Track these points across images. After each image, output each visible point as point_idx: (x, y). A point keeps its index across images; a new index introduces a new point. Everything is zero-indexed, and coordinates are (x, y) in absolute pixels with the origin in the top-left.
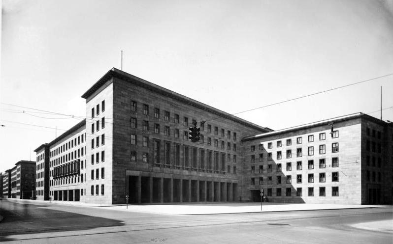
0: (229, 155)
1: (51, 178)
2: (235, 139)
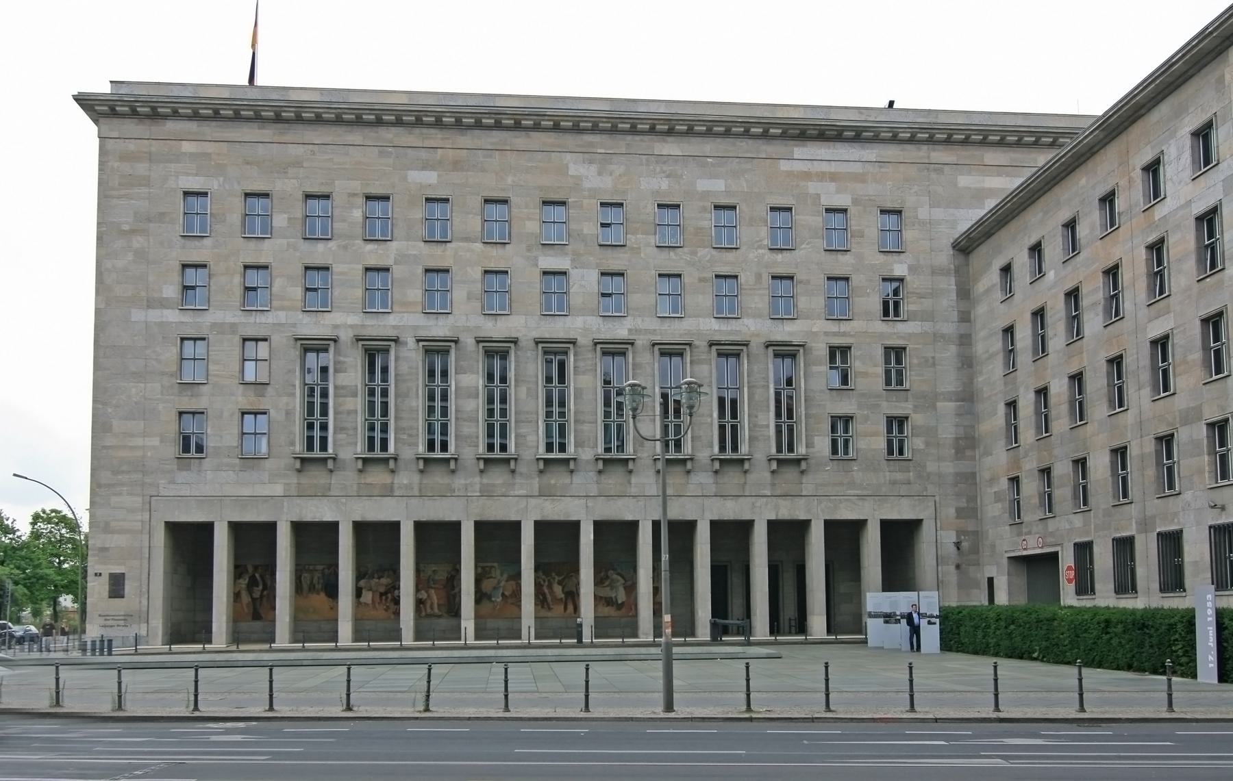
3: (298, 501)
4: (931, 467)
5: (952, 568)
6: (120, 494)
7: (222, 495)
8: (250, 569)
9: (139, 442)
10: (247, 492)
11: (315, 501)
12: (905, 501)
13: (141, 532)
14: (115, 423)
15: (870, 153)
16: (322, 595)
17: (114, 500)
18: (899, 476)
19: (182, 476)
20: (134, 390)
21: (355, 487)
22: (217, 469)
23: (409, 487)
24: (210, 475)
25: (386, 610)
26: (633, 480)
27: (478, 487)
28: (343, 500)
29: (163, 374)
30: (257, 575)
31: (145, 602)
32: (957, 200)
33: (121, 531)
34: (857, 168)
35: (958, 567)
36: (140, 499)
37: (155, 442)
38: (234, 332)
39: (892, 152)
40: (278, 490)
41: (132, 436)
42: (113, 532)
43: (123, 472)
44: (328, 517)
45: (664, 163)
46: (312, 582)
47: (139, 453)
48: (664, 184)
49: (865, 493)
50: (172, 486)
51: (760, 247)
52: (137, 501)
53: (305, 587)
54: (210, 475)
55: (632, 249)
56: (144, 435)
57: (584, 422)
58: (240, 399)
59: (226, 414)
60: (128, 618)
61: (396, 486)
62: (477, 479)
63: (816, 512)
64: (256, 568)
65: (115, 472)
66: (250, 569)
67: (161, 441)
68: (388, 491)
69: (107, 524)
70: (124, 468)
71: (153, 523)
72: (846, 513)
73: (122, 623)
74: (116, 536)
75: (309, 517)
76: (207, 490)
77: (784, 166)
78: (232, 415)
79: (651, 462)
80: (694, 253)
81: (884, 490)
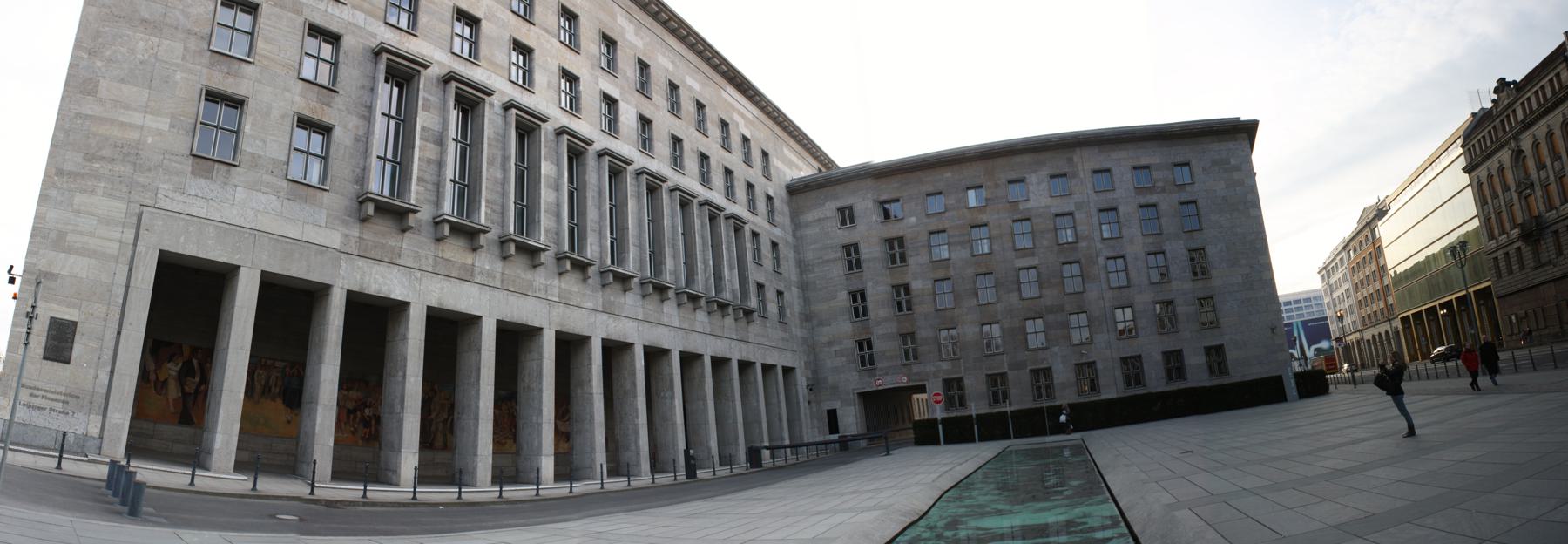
3: (360, 262)
6: (93, 192)
7: (260, 224)
8: (186, 352)
9: (136, 118)
10: (293, 232)
11: (382, 268)
12: (789, 354)
13: (116, 259)
14: (103, 84)
15: (756, 111)
16: (279, 401)
17: (79, 199)
19: (197, 185)
20: (141, 44)
21: (431, 260)
22: (253, 187)
23: (490, 275)
24: (241, 194)
25: (353, 433)
27: (556, 291)
28: (418, 274)
29: (189, 32)
30: (195, 361)
31: (104, 377)
32: (791, 164)
33: (83, 252)
36: (123, 206)
37: (163, 124)
38: (298, 12)
40: (334, 238)
41: (127, 107)
42: (69, 250)
43: (102, 158)
44: (398, 294)
46: (267, 382)
47: (135, 135)
48: (671, 67)
50: (178, 197)
52: (118, 208)
53: (258, 388)
54: (241, 194)
56: (146, 110)
57: (807, 225)
58: (297, 98)
59: (275, 113)
60: (71, 399)
61: (477, 270)
62: (556, 282)
63: (759, 357)
64: (194, 350)
65: (90, 157)
66: (186, 352)
67: (172, 126)
68: (467, 276)
69: (62, 235)
70: (106, 152)
71: (141, 248)
72: (770, 361)
73: (59, 406)
74: (72, 258)
75: (372, 289)
76: (232, 215)
78: (283, 117)
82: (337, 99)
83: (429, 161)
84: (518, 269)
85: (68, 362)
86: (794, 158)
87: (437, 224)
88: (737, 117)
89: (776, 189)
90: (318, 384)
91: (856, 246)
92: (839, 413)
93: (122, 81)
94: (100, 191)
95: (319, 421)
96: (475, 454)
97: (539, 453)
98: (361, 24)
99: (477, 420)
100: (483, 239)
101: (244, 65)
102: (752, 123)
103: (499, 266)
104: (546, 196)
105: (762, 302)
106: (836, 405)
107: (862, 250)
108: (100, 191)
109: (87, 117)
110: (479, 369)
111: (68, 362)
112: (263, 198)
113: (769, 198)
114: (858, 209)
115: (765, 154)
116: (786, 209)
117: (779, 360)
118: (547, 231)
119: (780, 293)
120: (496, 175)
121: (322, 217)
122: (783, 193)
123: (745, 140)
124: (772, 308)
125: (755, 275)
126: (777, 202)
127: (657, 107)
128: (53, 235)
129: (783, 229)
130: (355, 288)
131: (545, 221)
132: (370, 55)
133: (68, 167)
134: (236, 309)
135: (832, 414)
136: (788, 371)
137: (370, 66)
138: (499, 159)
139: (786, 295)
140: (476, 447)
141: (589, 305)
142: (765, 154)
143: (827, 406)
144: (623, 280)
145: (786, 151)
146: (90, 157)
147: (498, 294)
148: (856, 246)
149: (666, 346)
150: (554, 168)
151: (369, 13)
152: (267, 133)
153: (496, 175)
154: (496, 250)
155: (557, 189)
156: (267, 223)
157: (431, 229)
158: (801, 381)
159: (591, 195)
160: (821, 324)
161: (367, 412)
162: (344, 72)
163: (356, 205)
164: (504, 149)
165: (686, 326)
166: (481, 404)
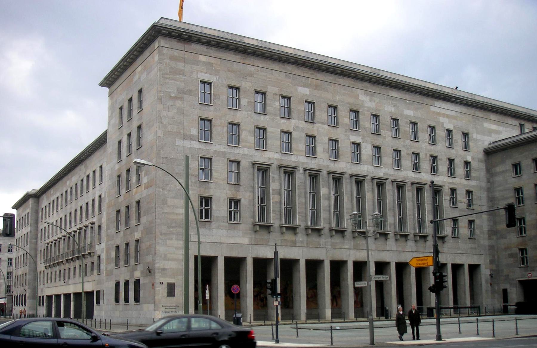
0: (453, 191)
1: (41, 267)
2: (466, 147)
4: (482, 242)
5: (489, 285)
6: (172, 239)
10: (232, 241)
12: (475, 257)
17: (169, 242)
18: (473, 246)
21: (280, 241)
22: (218, 228)
26: (388, 243)
33: (173, 260)
34: (454, 114)
35: (491, 284)
39: (464, 109)
40: (246, 241)
42: (168, 260)
43: (173, 227)
45: (393, 100)
48: (393, 110)
49: (463, 252)
51: (426, 142)
55: (383, 137)
58: (228, 191)
62: (329, 240)
65: (169, 227)
68: (294, 244)
69: (165, 255)
70: (173, 225)
72: (458, 261)
74: (170, 262)
77: (432, 109)
78: (224, 200)
79: (393, 235)
80: (404, 142)
81: (469, 252)
82: (241, 188)
83: (276, 202)
84: (314, 238)
85: (174, 296)
86: (494, 127)
87: (281, 227)
88: (442, 119)
89: (475, 155)
90: (246, 291)
91: (521, 189)
92: (509, 290)
93: (174, 198)
94: (174, 238)
95: (248, 302)
96: (300, 309)
97: (324, 308)
98: (247, 153)
99: (300, 297)
100: (298, 230)
101: (210, 183)
102: (455, 118)
103: (305, 238)
104: (324, 203)
105: (455, 230)
106: (507, 286)
107: (525, 192)
108: (174, 238)
109: (166, 213)
110: (300, 279)
111: (174, 296)
112: (221, 231)
113: (467, 164)
114: (523, 165)
115: (466, 135)
116: (483, 166)
117: (466, 261)
118: (324, 219)
119: (471, 222)
120: (302, 201)
121: (240, 233)
122: (481, 155)
123: (449, 131)
124: (464, 230)
125: (448, 212)
126: (474, 165)
127: (385, 138)
128: (163, 256)
129: (478, 179)
130: (254, 257)
131: (324, 215)
132: (251, 165)
133: (163, 232)
134: (219, 271)
135: (505, 291)
136: (474, 268)
137: (251, 169)
138: (303, 194)
139: (477, 222)
140: (300, 306)
141: (347, 247)
142: (466, 135)
143: (503, 286)
144: (405, 236)
145: (486, 125)
146: (169, 227)
147: (305, 249)
148: (521, 189)
149: (388, 261)
150: (327, 189)
151: (249, 148)
152: (220, 209)
153: (302, 201)
154: (304, 232)
155: (329, 199)
156: (224, 240)
157: (279, 229)
158: (485, 272)
159: (346, 198)
160: (497, 239)
161: (262, 295)
162: (243, 176)
163: (252, 226)
164: (254, 218)
165: (400, 249)
166: (301, 291)
